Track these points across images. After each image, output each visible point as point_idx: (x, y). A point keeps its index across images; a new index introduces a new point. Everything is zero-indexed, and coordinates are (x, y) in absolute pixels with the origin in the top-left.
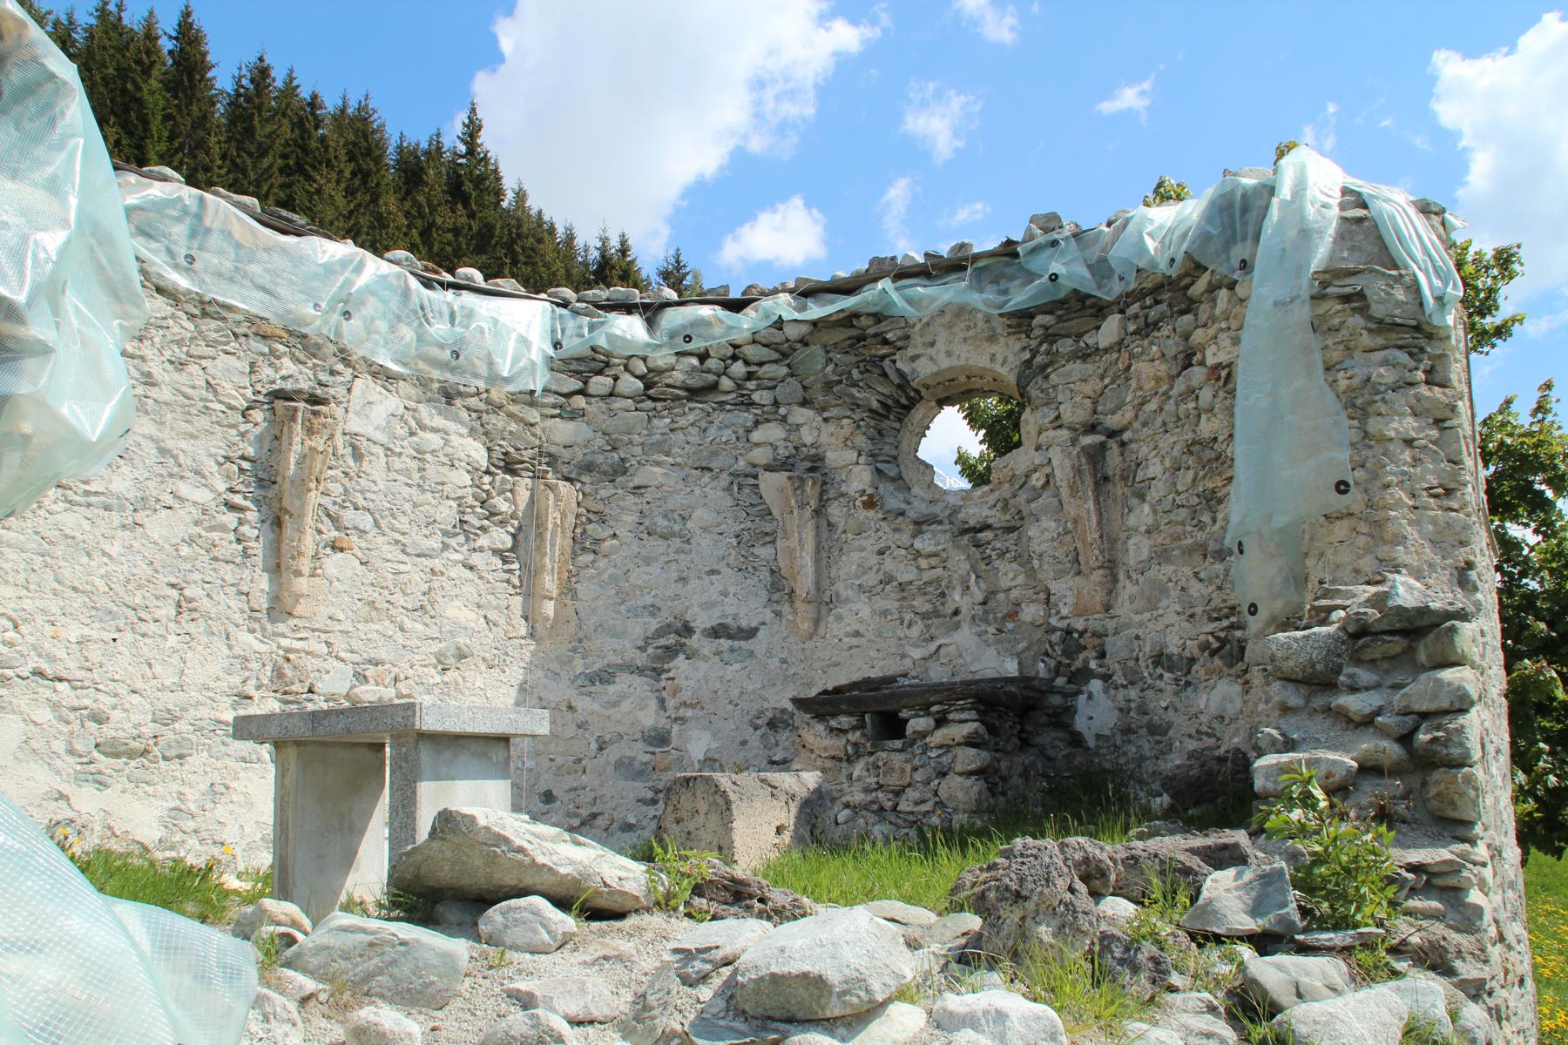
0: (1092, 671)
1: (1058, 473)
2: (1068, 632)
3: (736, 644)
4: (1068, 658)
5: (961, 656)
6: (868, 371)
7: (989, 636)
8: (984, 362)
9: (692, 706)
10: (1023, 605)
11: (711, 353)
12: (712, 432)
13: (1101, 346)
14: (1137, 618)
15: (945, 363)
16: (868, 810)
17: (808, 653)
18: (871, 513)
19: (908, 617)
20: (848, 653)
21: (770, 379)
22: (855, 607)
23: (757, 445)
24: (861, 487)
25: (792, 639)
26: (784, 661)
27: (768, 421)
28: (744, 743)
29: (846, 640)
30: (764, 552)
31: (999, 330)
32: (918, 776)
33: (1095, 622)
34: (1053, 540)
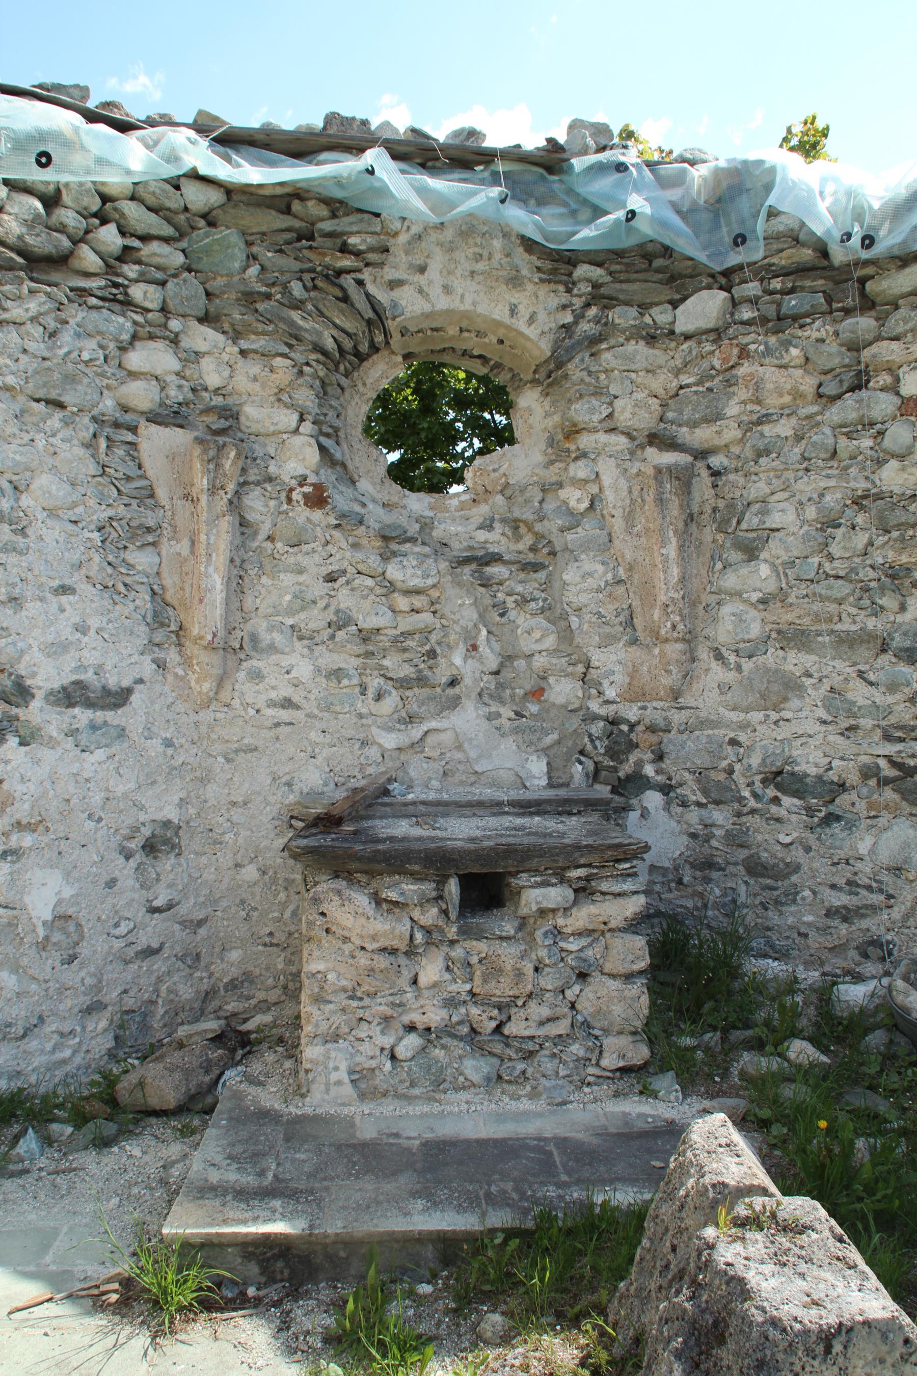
0: (647, 778)
1: (610, 496)
2: (614, 722)
3: (100, 716)
4: (612, 758)
5: (459, 747)
6: (315, 287)
7: (504, 721)
8: (500, 313)
9: (30, 828)
10: (551, 680)
11: (66, 198)
12: (66, 338)
13: (679, 328)
14: (735, 716)
15: (443, 303)
16: (454, 1036)
17: (204, 729)
18: (317, 515)
19: (375, 683)
20: (272, 734)
21: (158, 268)
22: (286, 661)
23: (133, 375)
24: (301, 471)
25: (180, 707)
26: (168, 743)
27: (151, 337)
28: (111, 883)
29: (270, 712)
30: (142, 559)
31: (525, 272)
32: (548, 981)
33: (654, 713)
34: (599, 590)
